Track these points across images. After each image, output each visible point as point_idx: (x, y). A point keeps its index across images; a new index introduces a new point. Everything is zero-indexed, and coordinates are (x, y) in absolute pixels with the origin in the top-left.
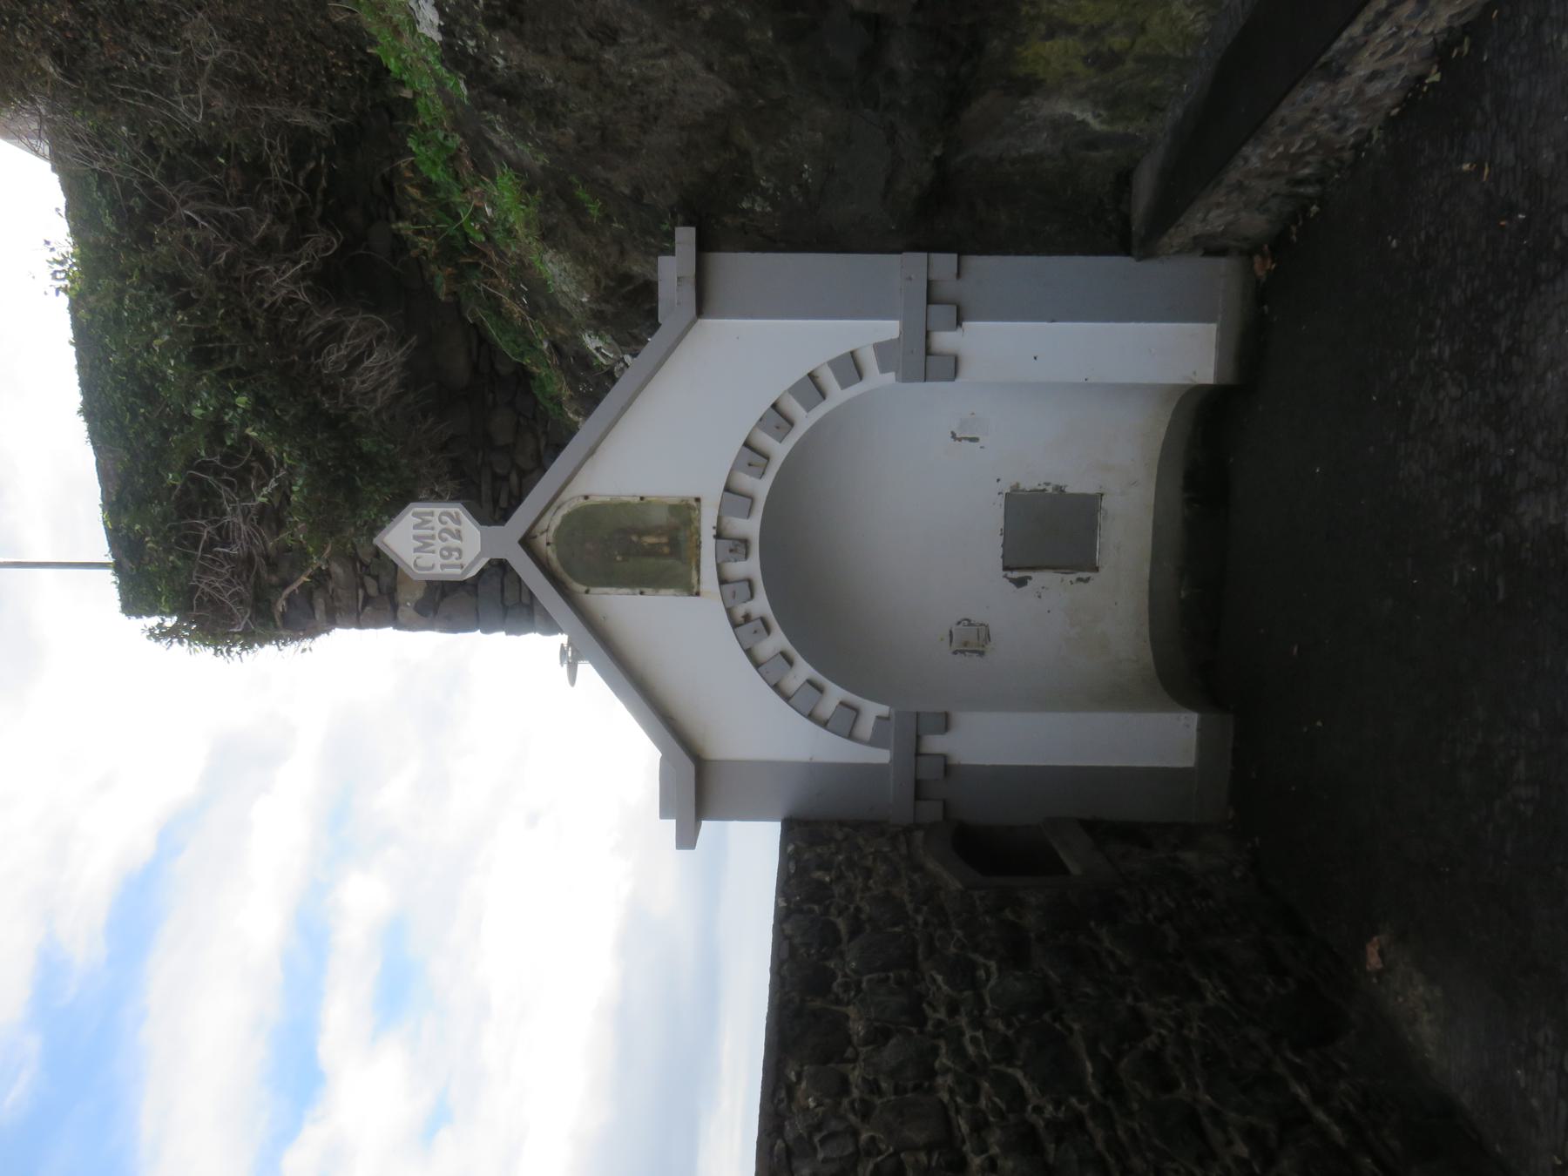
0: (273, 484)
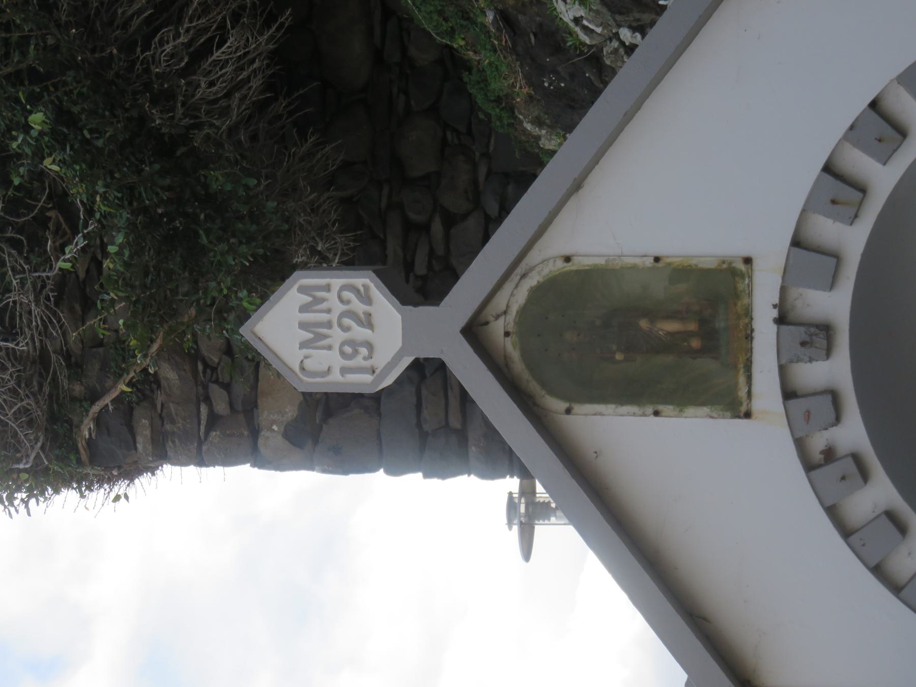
0: (80, 241)
